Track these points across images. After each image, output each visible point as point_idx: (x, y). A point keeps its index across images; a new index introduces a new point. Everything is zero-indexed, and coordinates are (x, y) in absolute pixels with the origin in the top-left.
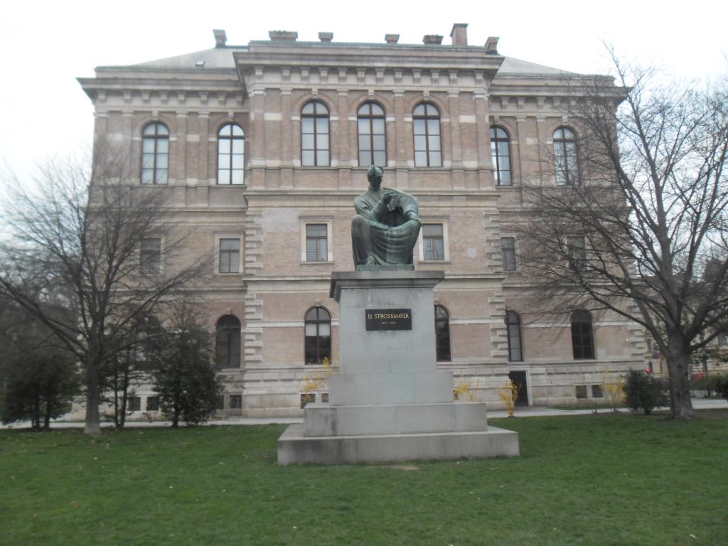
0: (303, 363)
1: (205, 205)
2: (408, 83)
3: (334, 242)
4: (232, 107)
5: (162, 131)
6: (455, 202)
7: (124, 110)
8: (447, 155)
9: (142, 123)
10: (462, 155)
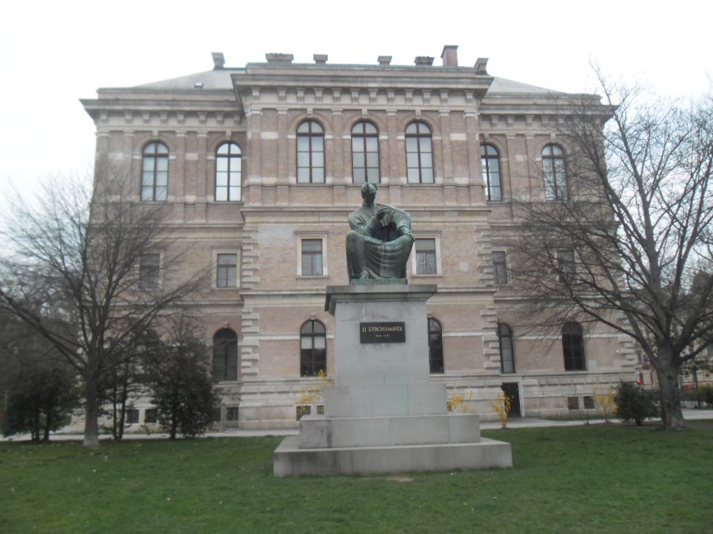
2: (400, 103)
3: (328, 256)
4: (229, 126)
5: (162, 150)
7: (125, 129)
8: (438, 172)
9: (142, 142)
10: (453, 171)
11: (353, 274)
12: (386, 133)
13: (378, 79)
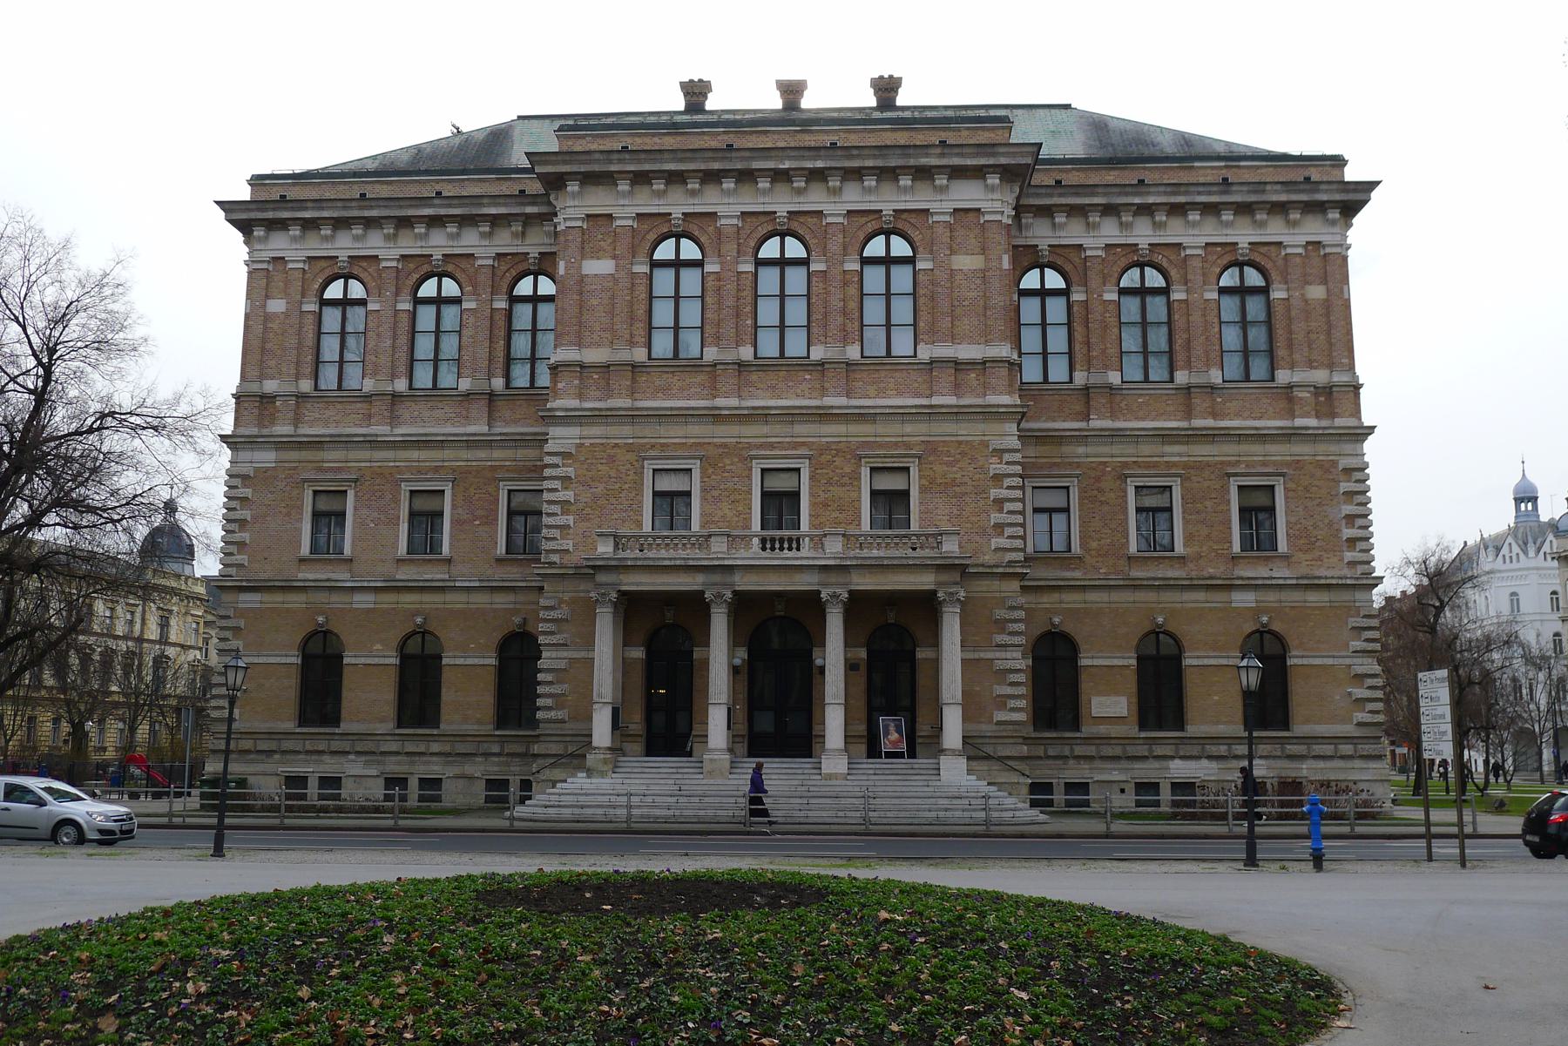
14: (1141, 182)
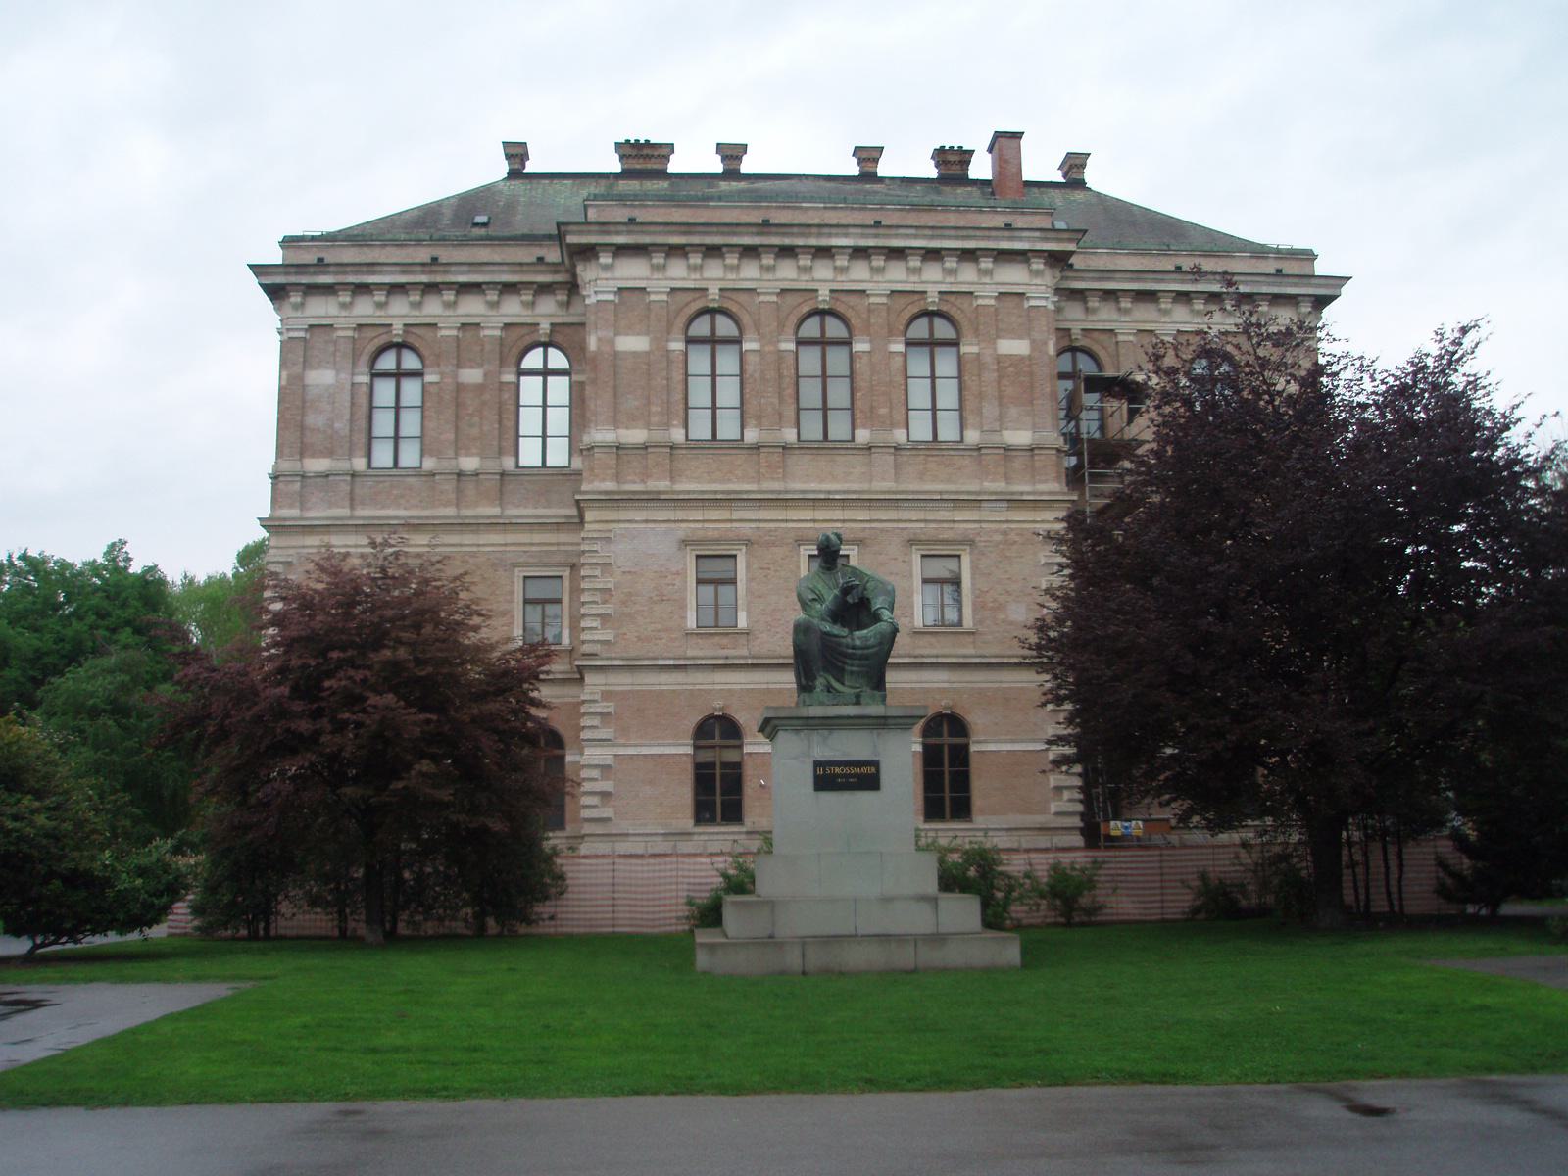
0: (691, 822)
1: (495, 511)
2: (897, 275)
3: (749, 591)
4: (548, 311)
5: (411, 362)
6: (984, 514)
7: (339, 322)
8: (971, 419)
9: (371, 348)
10: (1001, 418)
11: (803, 681)
12: (975, 341)
13: (851, 230)
14: (435, 260)
